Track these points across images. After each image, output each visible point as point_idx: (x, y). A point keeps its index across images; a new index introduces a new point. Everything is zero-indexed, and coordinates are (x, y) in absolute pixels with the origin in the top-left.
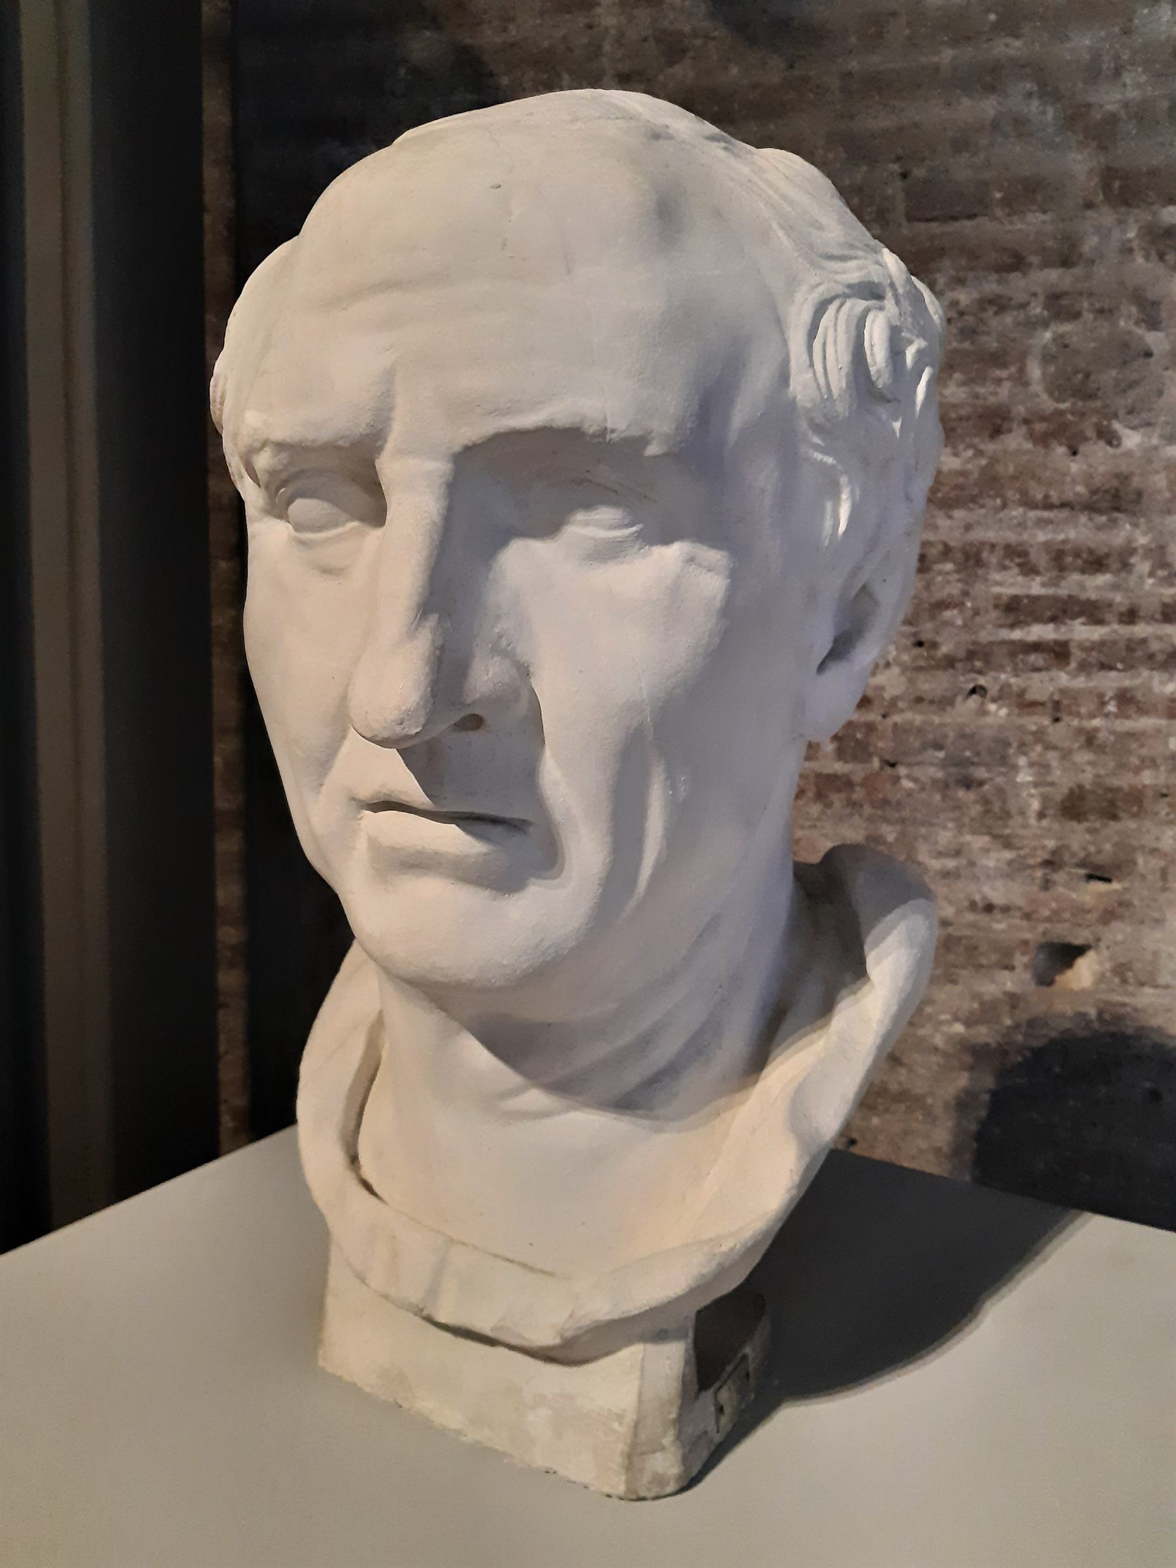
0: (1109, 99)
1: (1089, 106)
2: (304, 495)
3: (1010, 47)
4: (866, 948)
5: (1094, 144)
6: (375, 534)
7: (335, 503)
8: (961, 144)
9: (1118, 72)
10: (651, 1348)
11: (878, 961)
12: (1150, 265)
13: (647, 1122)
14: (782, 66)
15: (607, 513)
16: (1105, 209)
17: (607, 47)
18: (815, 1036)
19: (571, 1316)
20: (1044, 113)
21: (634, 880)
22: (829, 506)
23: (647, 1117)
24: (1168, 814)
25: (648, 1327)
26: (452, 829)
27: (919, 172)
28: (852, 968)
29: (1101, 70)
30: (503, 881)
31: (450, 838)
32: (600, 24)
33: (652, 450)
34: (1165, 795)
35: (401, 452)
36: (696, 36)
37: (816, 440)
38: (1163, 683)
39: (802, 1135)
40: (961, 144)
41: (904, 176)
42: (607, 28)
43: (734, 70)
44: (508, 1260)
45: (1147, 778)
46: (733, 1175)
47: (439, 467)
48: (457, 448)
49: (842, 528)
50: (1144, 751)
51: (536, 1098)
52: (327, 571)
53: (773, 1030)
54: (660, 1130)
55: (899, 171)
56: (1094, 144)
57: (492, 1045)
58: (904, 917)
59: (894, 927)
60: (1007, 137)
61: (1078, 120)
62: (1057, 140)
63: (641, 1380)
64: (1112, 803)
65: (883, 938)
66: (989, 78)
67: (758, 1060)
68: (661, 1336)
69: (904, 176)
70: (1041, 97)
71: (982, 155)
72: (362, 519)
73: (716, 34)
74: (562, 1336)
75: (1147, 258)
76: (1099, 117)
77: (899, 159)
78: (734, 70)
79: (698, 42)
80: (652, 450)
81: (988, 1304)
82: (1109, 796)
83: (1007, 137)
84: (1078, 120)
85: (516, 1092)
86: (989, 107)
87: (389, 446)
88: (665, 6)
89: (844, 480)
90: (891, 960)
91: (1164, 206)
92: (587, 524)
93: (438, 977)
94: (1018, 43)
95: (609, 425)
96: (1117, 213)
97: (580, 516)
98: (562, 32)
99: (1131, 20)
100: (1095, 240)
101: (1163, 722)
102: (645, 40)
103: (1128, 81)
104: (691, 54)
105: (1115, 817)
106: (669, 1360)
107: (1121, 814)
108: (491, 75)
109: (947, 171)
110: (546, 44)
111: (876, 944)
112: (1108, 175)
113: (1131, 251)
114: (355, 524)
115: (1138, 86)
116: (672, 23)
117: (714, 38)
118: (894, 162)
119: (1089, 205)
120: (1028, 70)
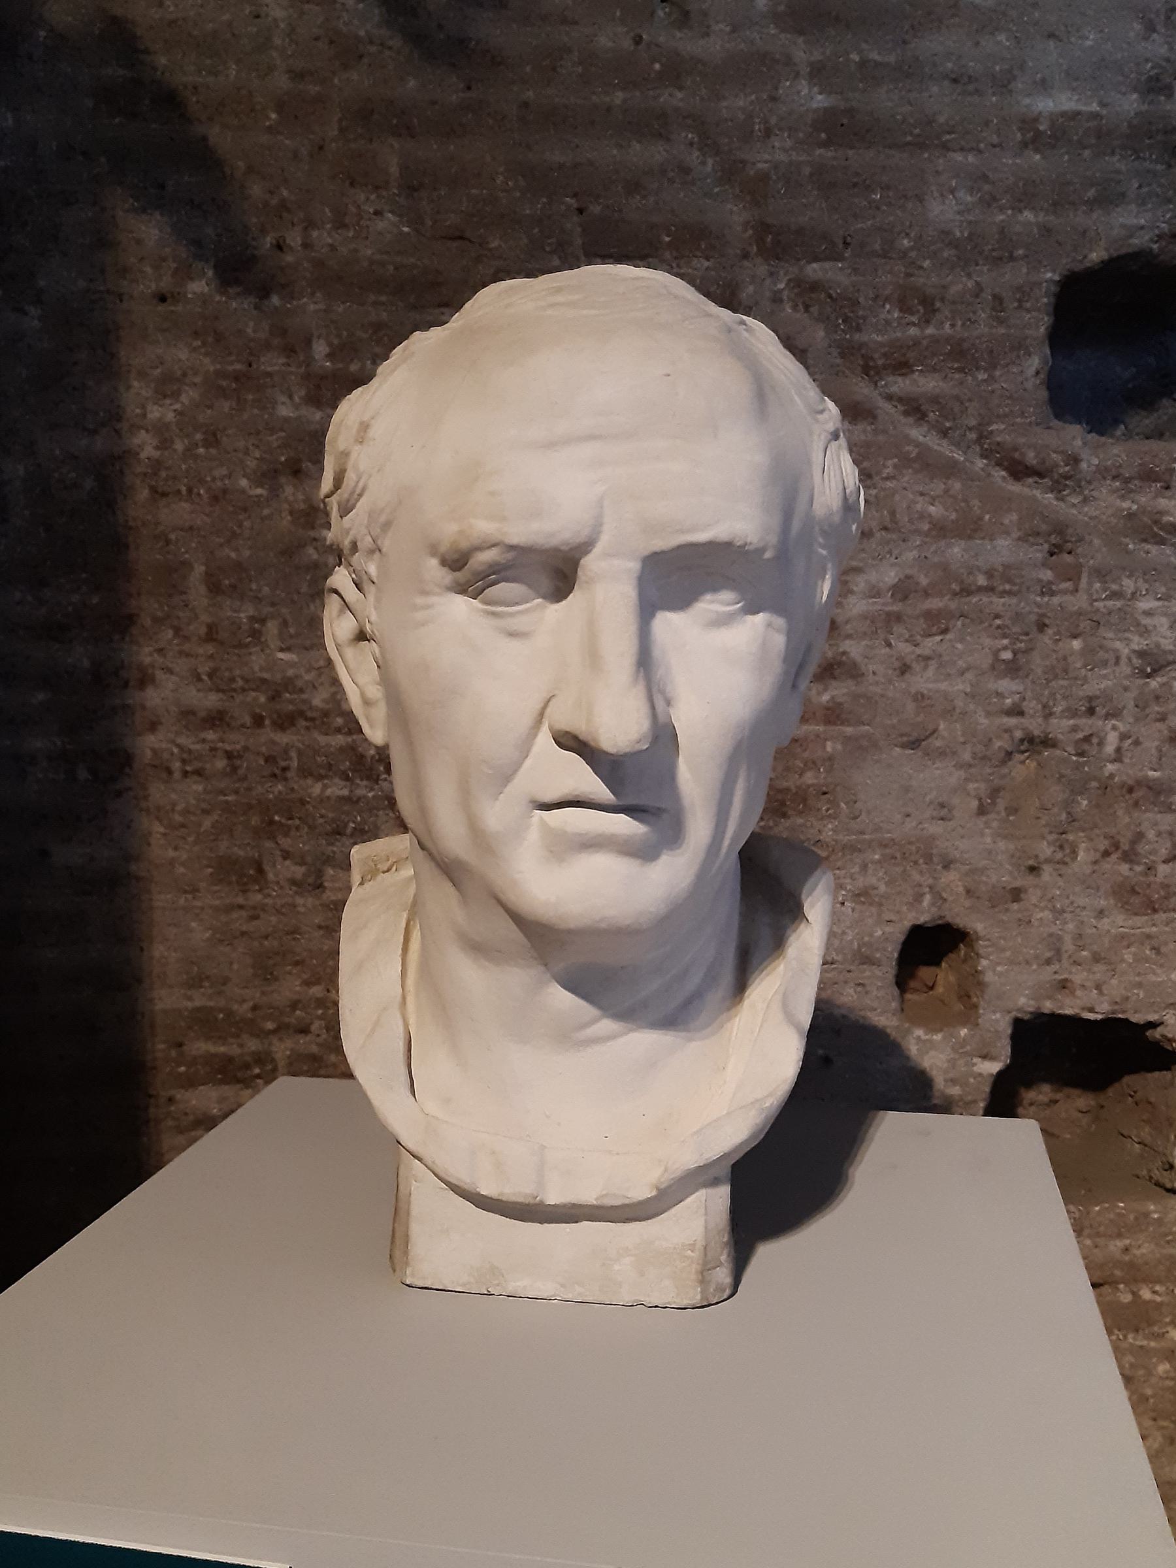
0: (764, 158)
1: (743, 162)
2: (507, 580)
3: (673, 98)
4: (803, 897)
5: (748, 198)
6: (555, 610)
7: (530, 586)
8: (634, 187)
9: (768, 133)
10: (710, 1191)
11: (812, 906)
12: (798, 315)
13: (683, 1034)
14: (462, 86)
15: (727, 595)
16: (759, 260)
17: (277, 41)
18: (774, 964)
19: (666, 1170)
20: (704, 163)
21: (720, 849)
22: (820, 583)
23: (684, 1030)
24: (827, 810)
25: (699, 1177)
26: (622, 817)
27: (596, 209)
28: (794, 912)
29: (752, 132)
30: (645, 853)
31: (622, 824)
32: (267, 15)
33: (768, 555)
34: (825, 793)
35: (607, 555)
36: (371, 42)
37: (821, 540)
38: (819, 694)
39: (797, 1026)
40: (634, 187)
41: (580, 211)
42: (275, 20)
43: (412, 83)
44: (393, 1236)
45: (809, 778)
46: (751, 1060)
47: (634, 566)
48: (646, 553)
49: (824, 598)
50: (806, 755)
51: (607, 1025)
52: (512, 634)
53: (746, 963)
54: (690, 1040)
55: (575, 206)
56: (748, 198)
57: (572, 986)
58: (824, 873)
59: (817, 885)
60: (671, 181)
61: (731, 171)
62: (716, 190)
63: (705, 1214)
64: (783, 803)
65: (813, 890)
66: (655, 126)
67: (740, 987)
68: (715, 1182)
69: (580, 211)
70: (700, 150)
71: (652, 199)
72: (544, 597)
73: (391, 43)
74: (658, 1189)
75: (795, 307)
76: (752, 173)
77: (575, 195)
78: (412, 83)
79: (373, 49)
80: (768, 555)
81: (851, 1171)
82: (780, 797)
83: (671, 181)
84: (731, 171)
85: (594, 1021)
86: (654, 153)
87: (597, 550)
88: (338, 6)
89: (829, 565)
90: (817, 907)
91: (809, 262)
92: (713, 602)
93: (603, 925)
94: (679, 95)
95: (749, 541)
96: (769, 265)
97: (708, 597)
98: (226, 17)
99: (777, 89)
100: (751, 289)
101: (821, 728)
102: (317, 39)
103: (776, 144)
104: (366, 60)
105: (784, 815)
106: (721, 1196)
107: (790, 813)
108: (147, 52)
109: (620, 211)
110: (210, 26)
111: (810, 894)
112: (762, 228)
113: (781, 301)
114: (540, 600)
115: (785, 150)
116: (346, 24)
117: (390, 48)
118: (572, 198)
119: (746, 256)
120: (690, 121)
